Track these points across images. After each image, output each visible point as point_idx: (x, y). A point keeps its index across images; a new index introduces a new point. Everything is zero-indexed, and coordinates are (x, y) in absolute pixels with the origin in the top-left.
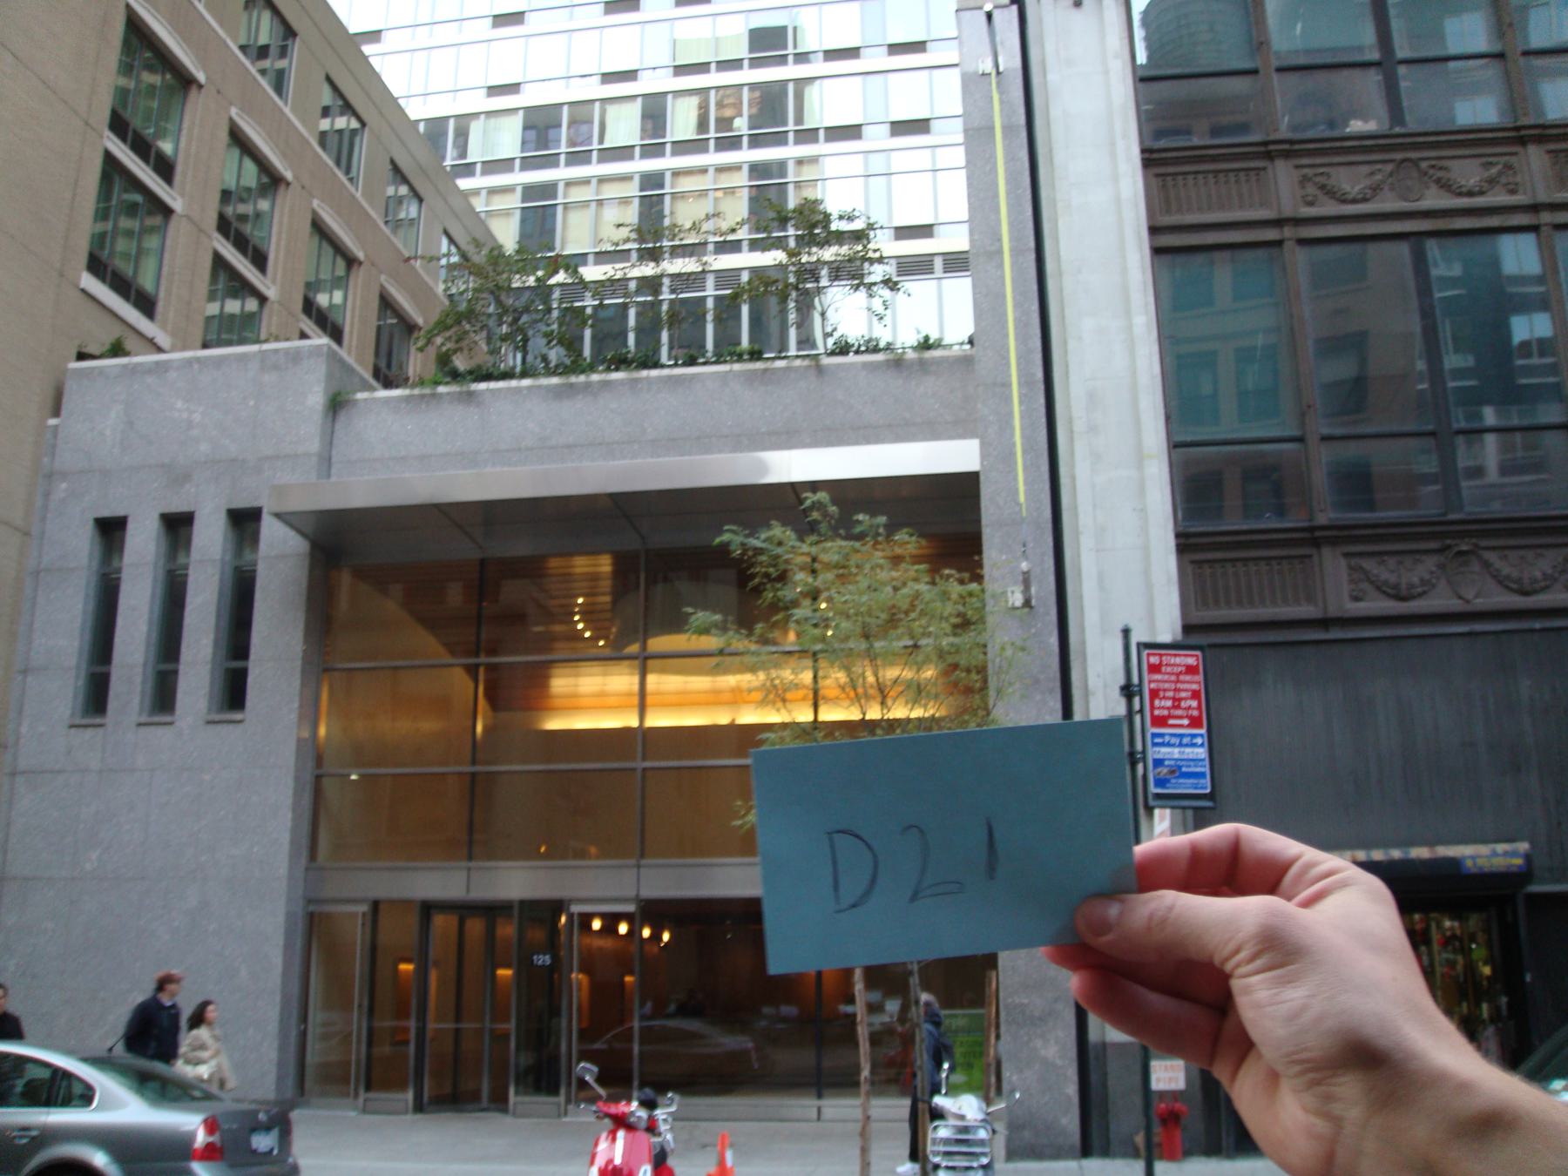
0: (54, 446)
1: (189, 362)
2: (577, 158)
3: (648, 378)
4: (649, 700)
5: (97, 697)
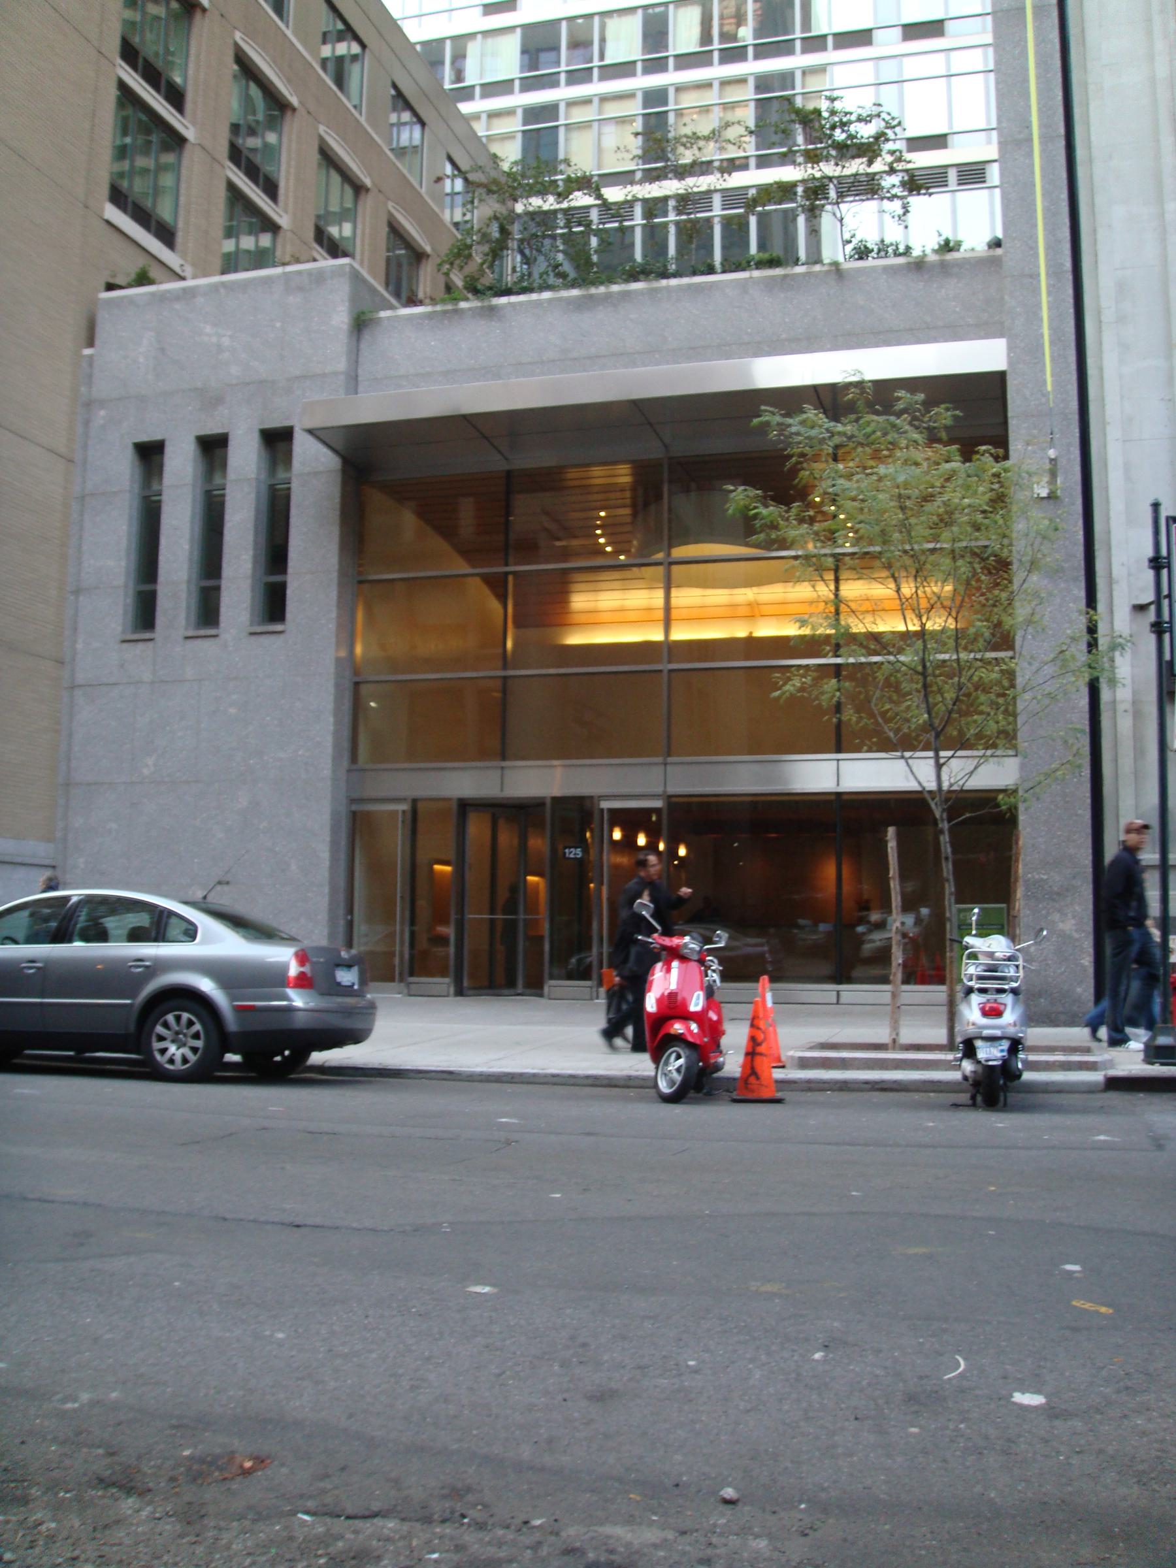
0: (90, 376)
1: (215, 288)
2: (578, 77)
3: (667, 288)
4: (674, 614)
5: (145, 613)
